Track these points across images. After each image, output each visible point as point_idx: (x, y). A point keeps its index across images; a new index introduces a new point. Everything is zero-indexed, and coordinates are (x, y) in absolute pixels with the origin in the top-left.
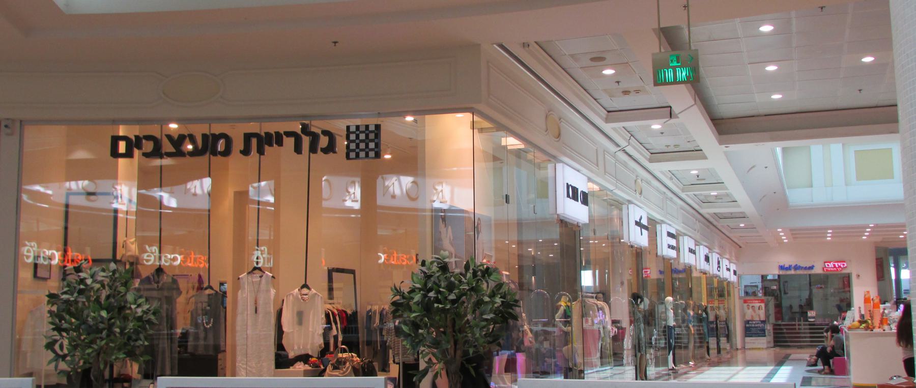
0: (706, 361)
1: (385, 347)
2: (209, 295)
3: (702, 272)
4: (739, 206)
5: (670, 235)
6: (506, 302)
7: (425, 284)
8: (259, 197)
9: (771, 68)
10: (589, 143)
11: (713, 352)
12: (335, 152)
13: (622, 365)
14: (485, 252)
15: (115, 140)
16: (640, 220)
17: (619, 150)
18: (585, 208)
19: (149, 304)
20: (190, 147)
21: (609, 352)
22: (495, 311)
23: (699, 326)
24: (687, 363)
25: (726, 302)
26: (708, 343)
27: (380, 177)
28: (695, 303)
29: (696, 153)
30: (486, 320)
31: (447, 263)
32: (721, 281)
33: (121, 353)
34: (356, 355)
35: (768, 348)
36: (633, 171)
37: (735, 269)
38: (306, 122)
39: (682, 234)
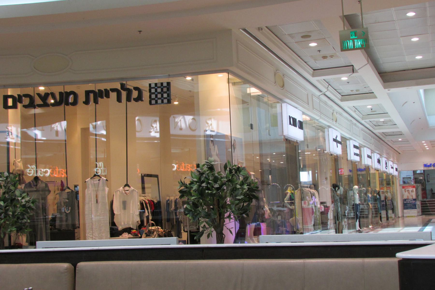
0: (379, 225)
1: (179, 222)
2: (68, 192)
3: (376, 170)
4: (398, 128)
5: (355, 147)
6: (251, 188)
7: (200, 179)
8: (96, 131)
9: (415, 39)
10: (301, 89)
11: (384, 220)
12: (142, 101)
13: (327, 229)
14: (239, 161)
15: (6, 98)
16: (336, 138)
17: (322, 94)
18: (301, 131)
19: (29, 197)
20: (52, 101)
21: (319, 221)
22: (244, 194)
23: (375, 204)
24: (367, 227)
25: (391, 188)
26: (380, 213)
27: (172, 116)
28: (372, 189)
29: (370, 95)
30: (239, 200)
31: (213, 165)
32: (388, 175)
33: (14, 227)
34: (160, 228)
35: (418, 216)
36: (331, 107)
37: (397, 168)
38: (124, 82)
39: (363, 146)
